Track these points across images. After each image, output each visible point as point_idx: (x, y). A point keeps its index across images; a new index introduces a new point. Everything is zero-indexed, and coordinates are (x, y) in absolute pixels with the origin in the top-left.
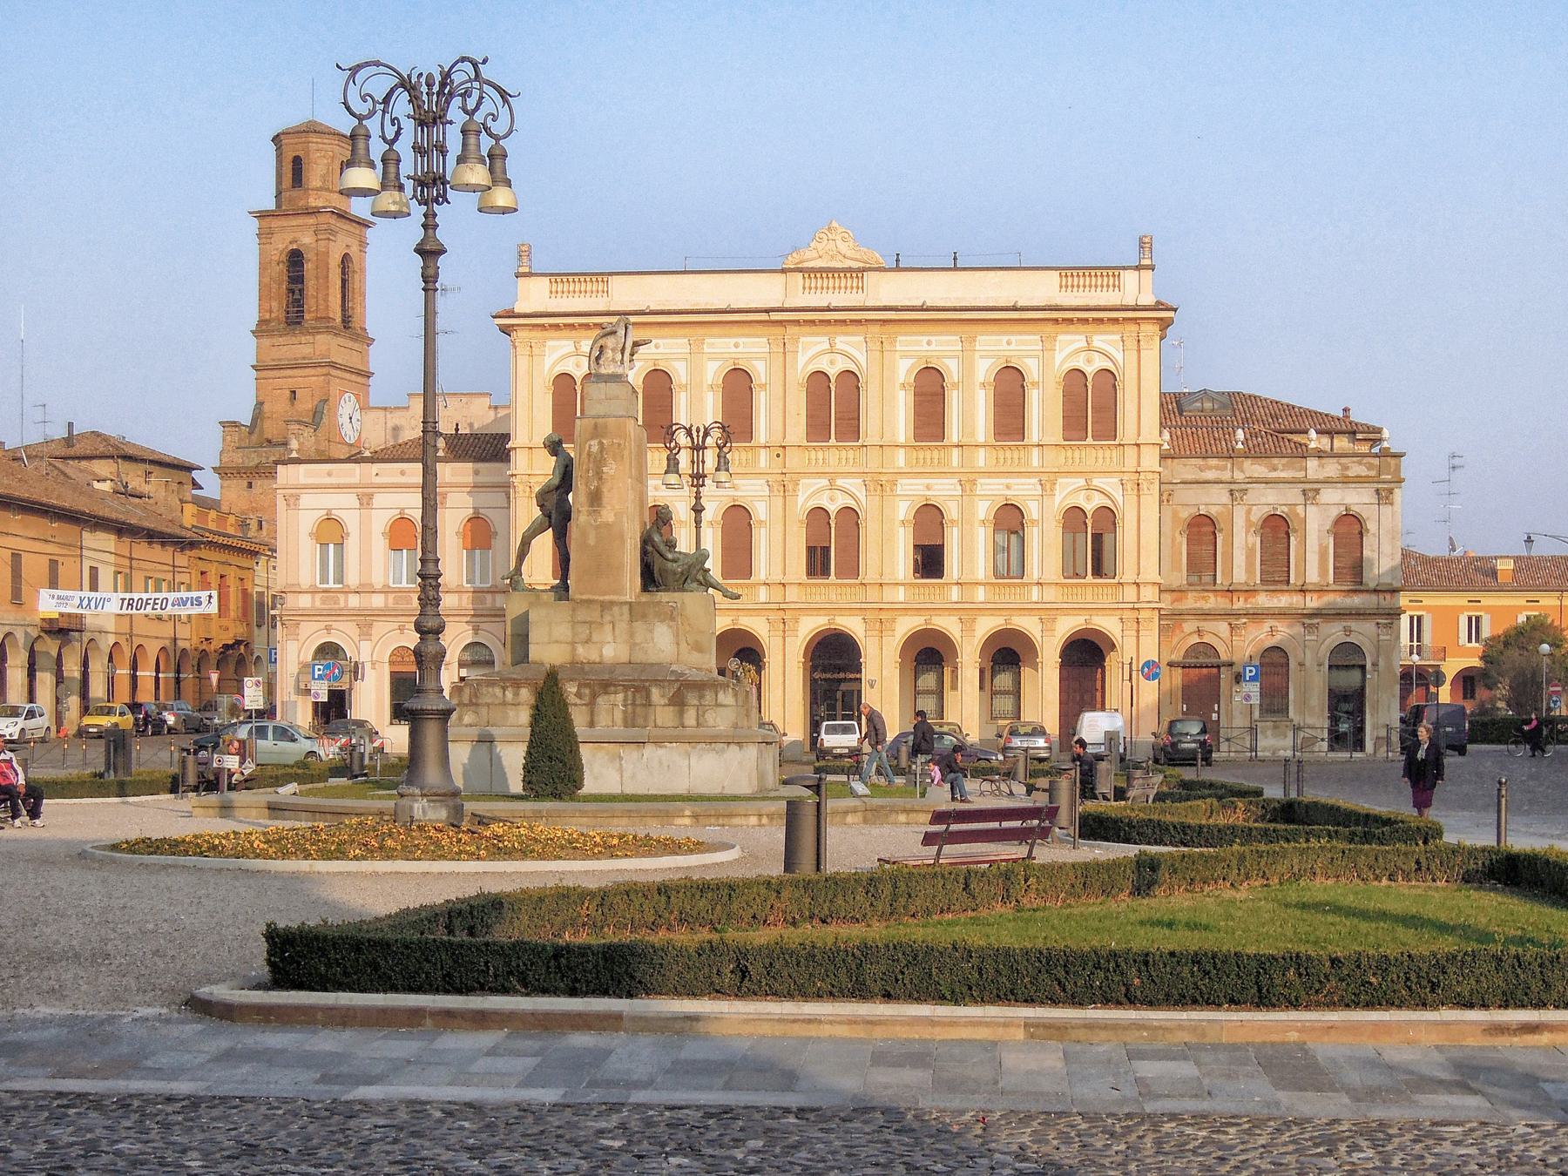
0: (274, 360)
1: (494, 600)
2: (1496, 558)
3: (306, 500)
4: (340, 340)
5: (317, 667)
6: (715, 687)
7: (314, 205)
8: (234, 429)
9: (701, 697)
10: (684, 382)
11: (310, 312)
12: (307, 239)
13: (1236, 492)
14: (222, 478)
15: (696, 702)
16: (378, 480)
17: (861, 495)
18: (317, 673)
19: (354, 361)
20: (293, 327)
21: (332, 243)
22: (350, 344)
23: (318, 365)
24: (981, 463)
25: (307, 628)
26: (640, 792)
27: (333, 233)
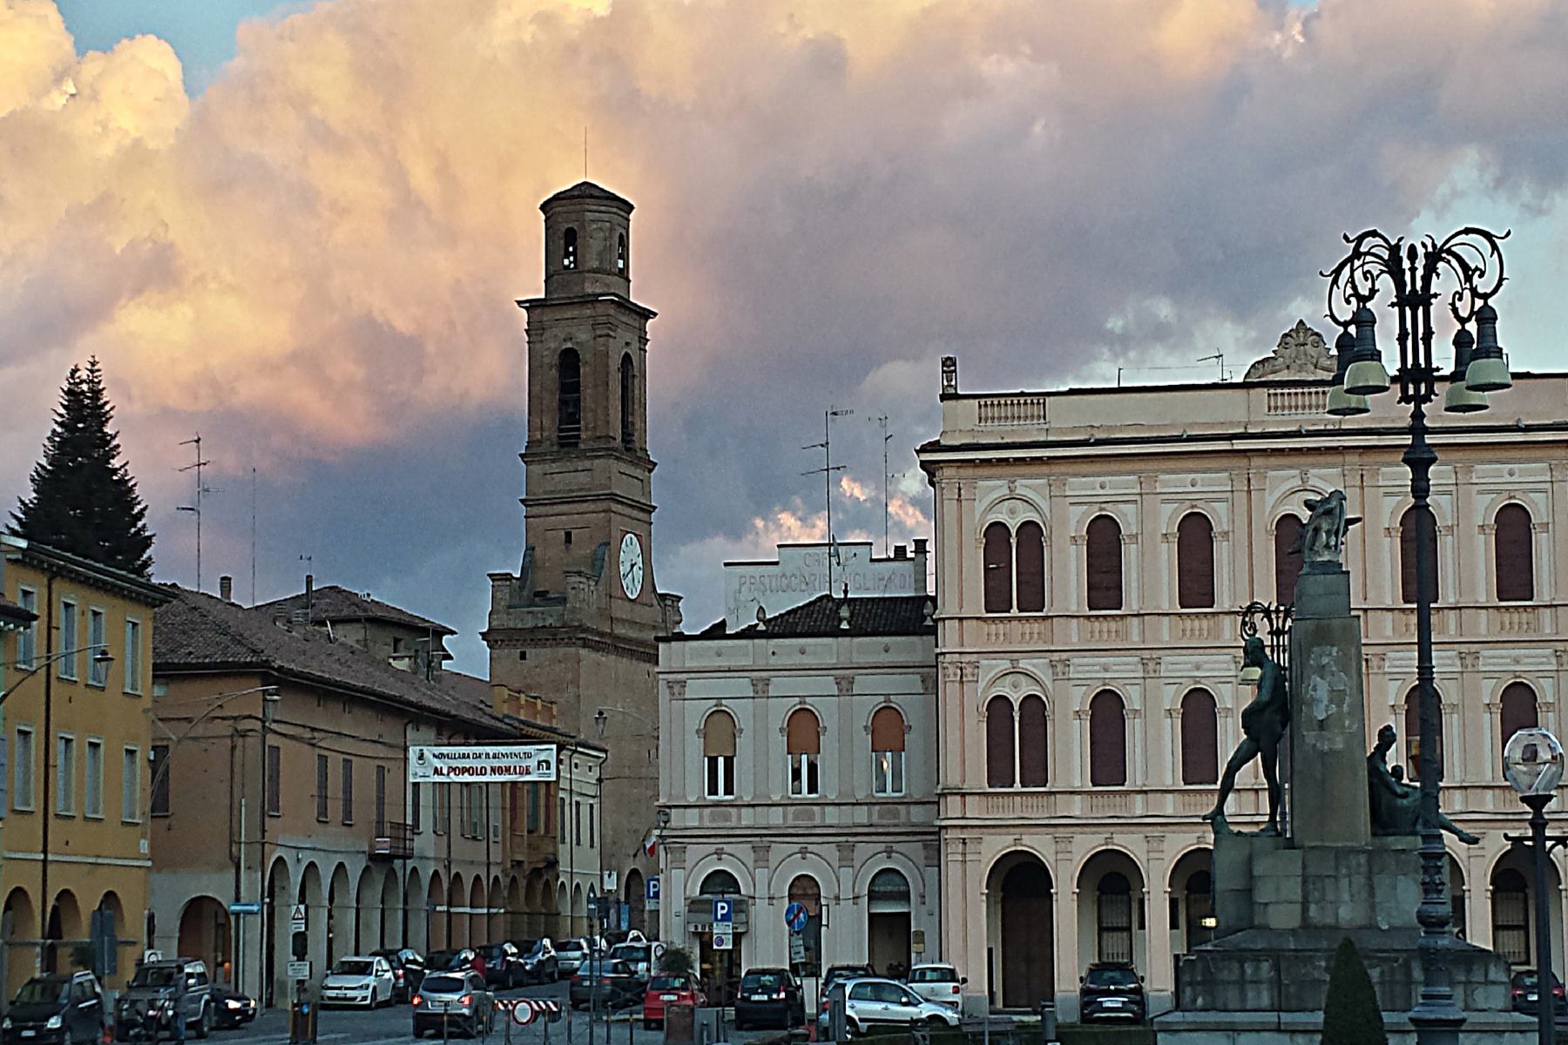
0: (545, 493)
1: (908, 813)
3: (695, 687)
4: (624, 467)
5: (719, 905)
7: (590, 291)
8: (504, 583)
9: (1469, 971)
10: (1134, 532)
11: (587, 429)
12: (583, 335)
15: (1463, 979)
16: (774, 662)
18: (720, 912)
20: (566, 449)
21: (611, 340)
22: (631, 470)
23: (597, 499)
24: (1483, 629)
25: (694, 851)
27: (611, 326)
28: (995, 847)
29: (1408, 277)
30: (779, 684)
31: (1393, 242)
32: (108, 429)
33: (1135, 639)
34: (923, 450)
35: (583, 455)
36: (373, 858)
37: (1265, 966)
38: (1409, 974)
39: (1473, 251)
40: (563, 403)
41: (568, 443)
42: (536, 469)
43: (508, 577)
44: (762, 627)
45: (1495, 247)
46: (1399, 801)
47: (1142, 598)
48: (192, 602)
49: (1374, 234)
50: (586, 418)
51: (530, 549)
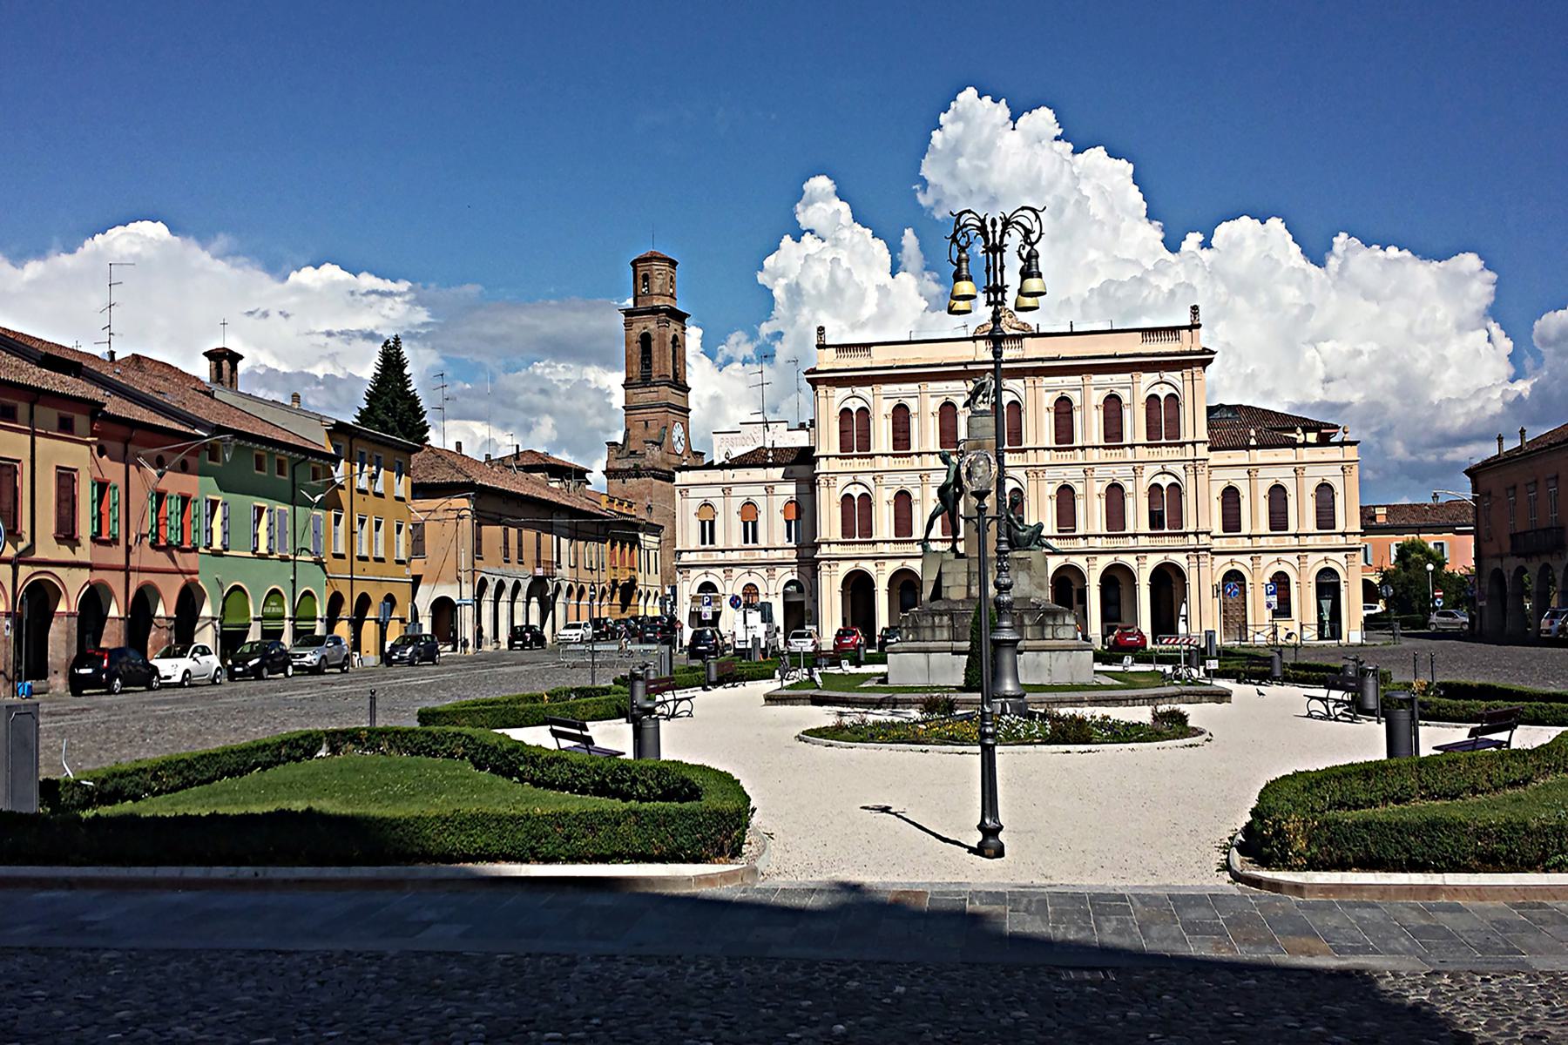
2: (1374, 507)
6: (1053, 614)
9: (1055, 619)
13: (1298, 468)
14: (608, 478)
17: (1024, 479)
18: (705, 602)
19: (680, 403)
26: (77, 570)
28: (845, 568)
29: (991, 236)
30: (735, 490)
31: (982, 217)
32: (406, 371)
33: (917, 465)
34: (806, 373)
35: (653, 385)
36: (535, 578)
37: (945, 618)
38: (1022, 621)
39: (1027, 219)
40: (643, 359)
41: (646, 381)
42: (631, 391)
43: (615, 444)
44: (728, 462)
45: (1037, 217)
46: (1021, 533)
47: (921, 444)
48: (439, 453)
49: (969, 211)
50: (655, 366)
51: (627, 430)
